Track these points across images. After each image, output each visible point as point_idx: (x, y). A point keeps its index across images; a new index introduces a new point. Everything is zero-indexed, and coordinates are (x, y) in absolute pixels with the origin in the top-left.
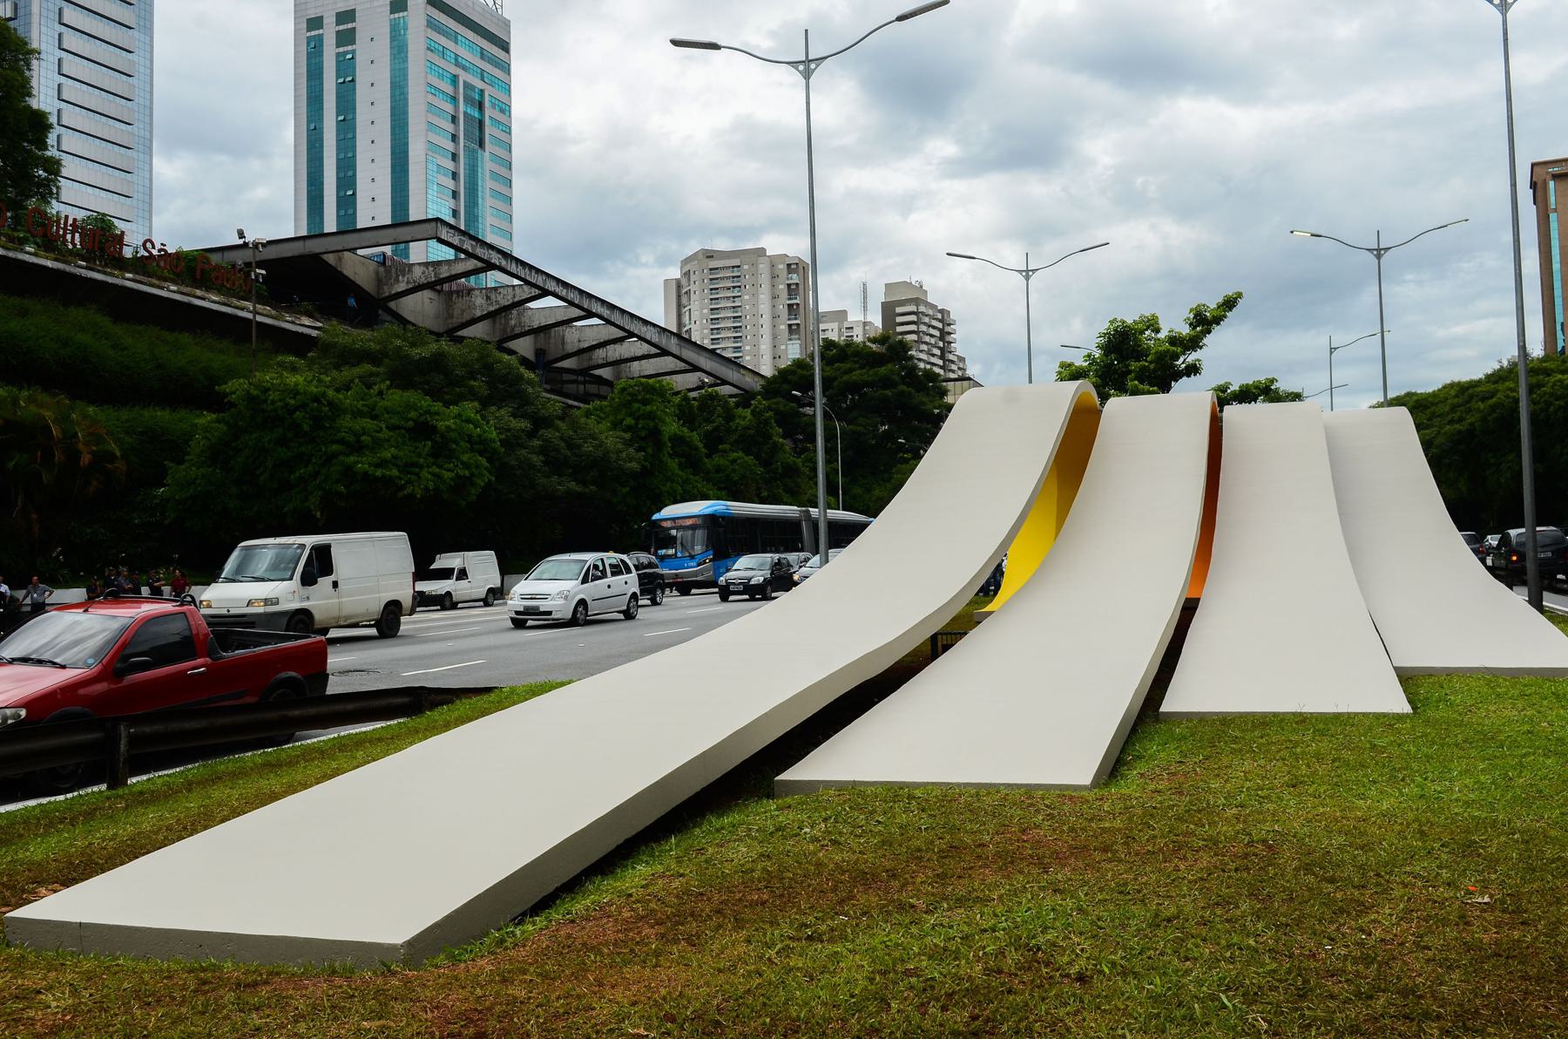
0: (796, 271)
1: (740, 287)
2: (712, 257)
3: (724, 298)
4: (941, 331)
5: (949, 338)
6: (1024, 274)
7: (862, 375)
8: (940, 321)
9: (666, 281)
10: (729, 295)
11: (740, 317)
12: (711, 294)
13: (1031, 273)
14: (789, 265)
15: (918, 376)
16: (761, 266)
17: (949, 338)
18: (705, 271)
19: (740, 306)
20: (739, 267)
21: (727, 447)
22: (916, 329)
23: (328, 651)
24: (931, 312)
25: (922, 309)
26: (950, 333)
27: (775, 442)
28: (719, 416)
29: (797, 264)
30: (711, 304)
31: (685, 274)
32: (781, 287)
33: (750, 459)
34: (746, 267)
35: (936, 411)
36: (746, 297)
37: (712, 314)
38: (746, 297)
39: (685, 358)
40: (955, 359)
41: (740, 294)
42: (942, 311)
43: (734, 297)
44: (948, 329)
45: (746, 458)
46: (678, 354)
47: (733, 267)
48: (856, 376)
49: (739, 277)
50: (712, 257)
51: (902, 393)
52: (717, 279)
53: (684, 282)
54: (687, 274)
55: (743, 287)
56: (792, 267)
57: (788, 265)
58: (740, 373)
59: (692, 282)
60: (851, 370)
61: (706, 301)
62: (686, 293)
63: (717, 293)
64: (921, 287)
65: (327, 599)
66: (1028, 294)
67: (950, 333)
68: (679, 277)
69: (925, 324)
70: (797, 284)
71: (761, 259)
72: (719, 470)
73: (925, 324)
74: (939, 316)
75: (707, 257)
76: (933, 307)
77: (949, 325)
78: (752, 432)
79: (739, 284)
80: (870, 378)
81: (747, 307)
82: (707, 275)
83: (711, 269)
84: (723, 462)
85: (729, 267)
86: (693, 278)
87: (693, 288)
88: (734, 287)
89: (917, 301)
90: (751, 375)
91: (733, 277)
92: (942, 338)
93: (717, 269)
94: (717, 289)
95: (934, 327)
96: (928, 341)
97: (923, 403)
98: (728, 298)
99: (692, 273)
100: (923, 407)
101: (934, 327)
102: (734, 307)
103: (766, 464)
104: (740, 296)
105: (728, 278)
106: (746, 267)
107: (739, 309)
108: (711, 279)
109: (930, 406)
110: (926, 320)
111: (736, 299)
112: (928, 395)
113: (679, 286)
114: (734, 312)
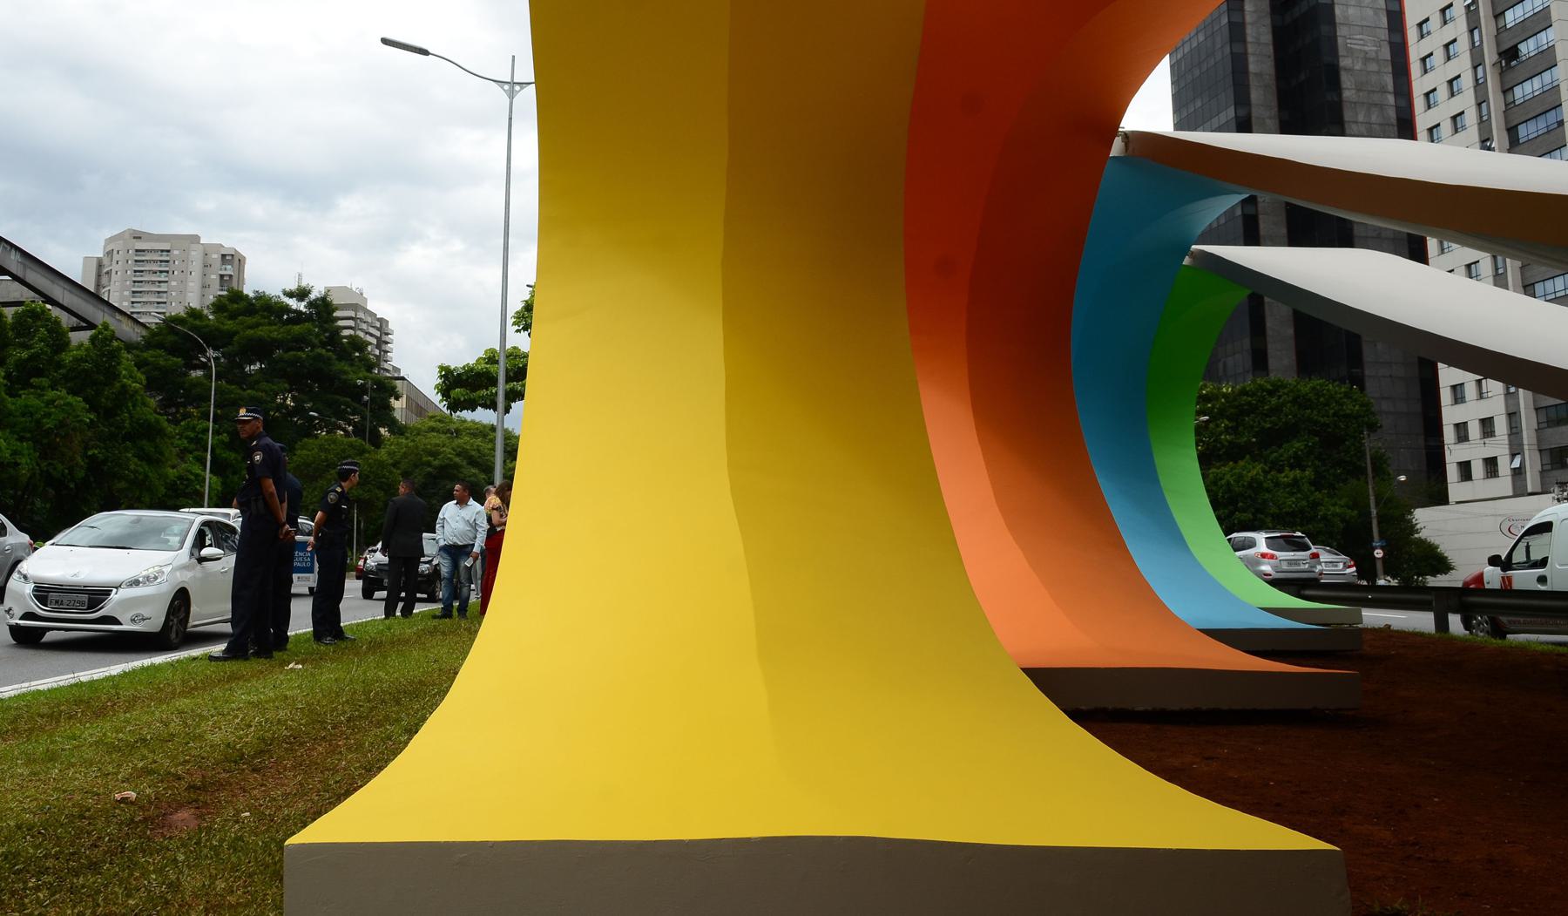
0: (231, 262)
1: (167, 272)
2: (140, 238)
3: (148, 282)
4: (378, 339)
5: (385, 347)
6: (506, 87)
7: (271, 332)
8: (378, 329)
9: (86, 258)
10: (153, 279)
11: (165, 303)
12: (135, 276)
13: (517, 88)
14: (224, 256)
15: (342, 343)
16: (193, 253)
17: (385, 347)
18: (130, 252)
19: (166, 292)
20: (168, 251)
21: (45, 381)
22: (354, 316)
23: (226, 608)
24: (369, 320)
25: (361, 315)
26: (387, 343)
27: (124, 386)
28: (41, 340)
29: (232, 255)
30: (134, 286)
31: (108, 253)
32: (213, 277)
33: (77, 401)
34: (176, 252)
35: (360, 382)
36: (174, 283)
37: (133, 297)
38: (174, 283)
39: (30, 282)
40: (390, 368)
41: (167, 279)
42: (381, 320)
43: (160, 282)
44: (385, 338)
45: (70, 399)
46: (20, 274)
47: (162, 251)
48: (262, 332)
49: (167, 261)
50: (140, 238)
51: (319, 357)
52: (143, 261)
53: (106, 262)
54: (110, 253)
55: (171, 273)
56: (227, 258)
57: (223, 255)
58: (114, 318)
59: (114, 262)
60: (257, 325)
61: (128, 283)
62: (107, 273)
63: (142, 276)
64: (362, 294)
65: (1316, 625)
66: (510, 119)
67: (387, 343)
68: (102, 256)
69: (362, 330)
70: (231, 276)
71: (194, 246)
72: (27, 412)
73: (362, 330)
74: (378, 325)
75: (134, 238)
76: (373, 315)
77: (387, 334)
78: (87, 366)
79: (167, 269)
80: (279, 336)
81: (174, 294)
82: (132, 256)
83: (137, 251)
84: (33, 401)
85: (158, 251)
86: (116, 256)
87: (114, 267)
88: (161, 272)
89: (355, 307)
90: (130, 323)
91: (161, 261)
92: (378, 346)
93: (144, 251)
94: (142, 271)
95: (371, 335)
96: (365, 328)
97: (345, 373)
98: (153, 282)
99: (115, 252)
100: (344, 377)
101: (371, 335)
102: (159, 292)
103: (108, 414)
104: (167, 282)
105: (155, 261)
106: (176, 252)
107: (165, 295)
108: (136, 261)
109: (351, 376)
110: (364, 326)
111: (162, 284)
112: (352, 365)
113: (100, 265)
114: (158, 297)
